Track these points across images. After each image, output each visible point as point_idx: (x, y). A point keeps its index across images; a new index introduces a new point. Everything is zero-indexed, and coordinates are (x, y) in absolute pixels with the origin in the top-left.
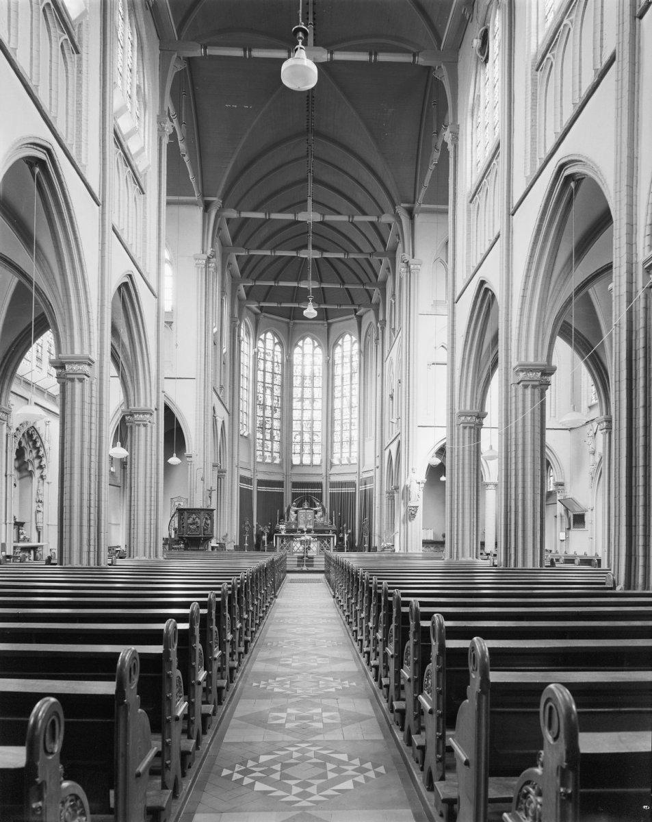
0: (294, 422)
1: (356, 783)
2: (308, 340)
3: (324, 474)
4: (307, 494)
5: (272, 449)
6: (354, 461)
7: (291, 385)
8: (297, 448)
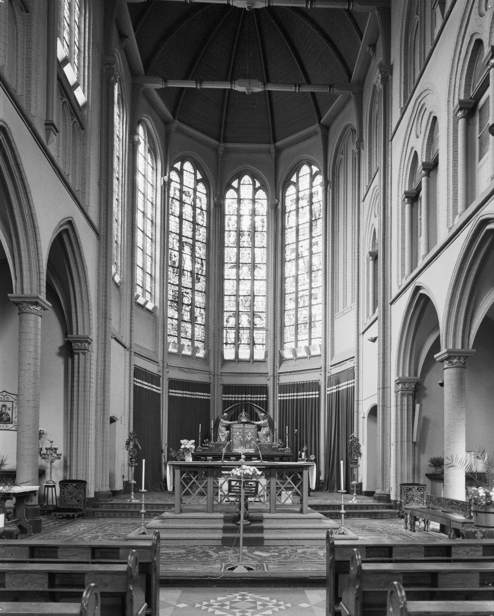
0: (226, 298)
1: (274, 612)
2: (247, 179)
3: (271, 373)
4: (245, 400)
5: (193, 335)
6: (316, 351)
7: (222, 245)
8: (230, 336)
